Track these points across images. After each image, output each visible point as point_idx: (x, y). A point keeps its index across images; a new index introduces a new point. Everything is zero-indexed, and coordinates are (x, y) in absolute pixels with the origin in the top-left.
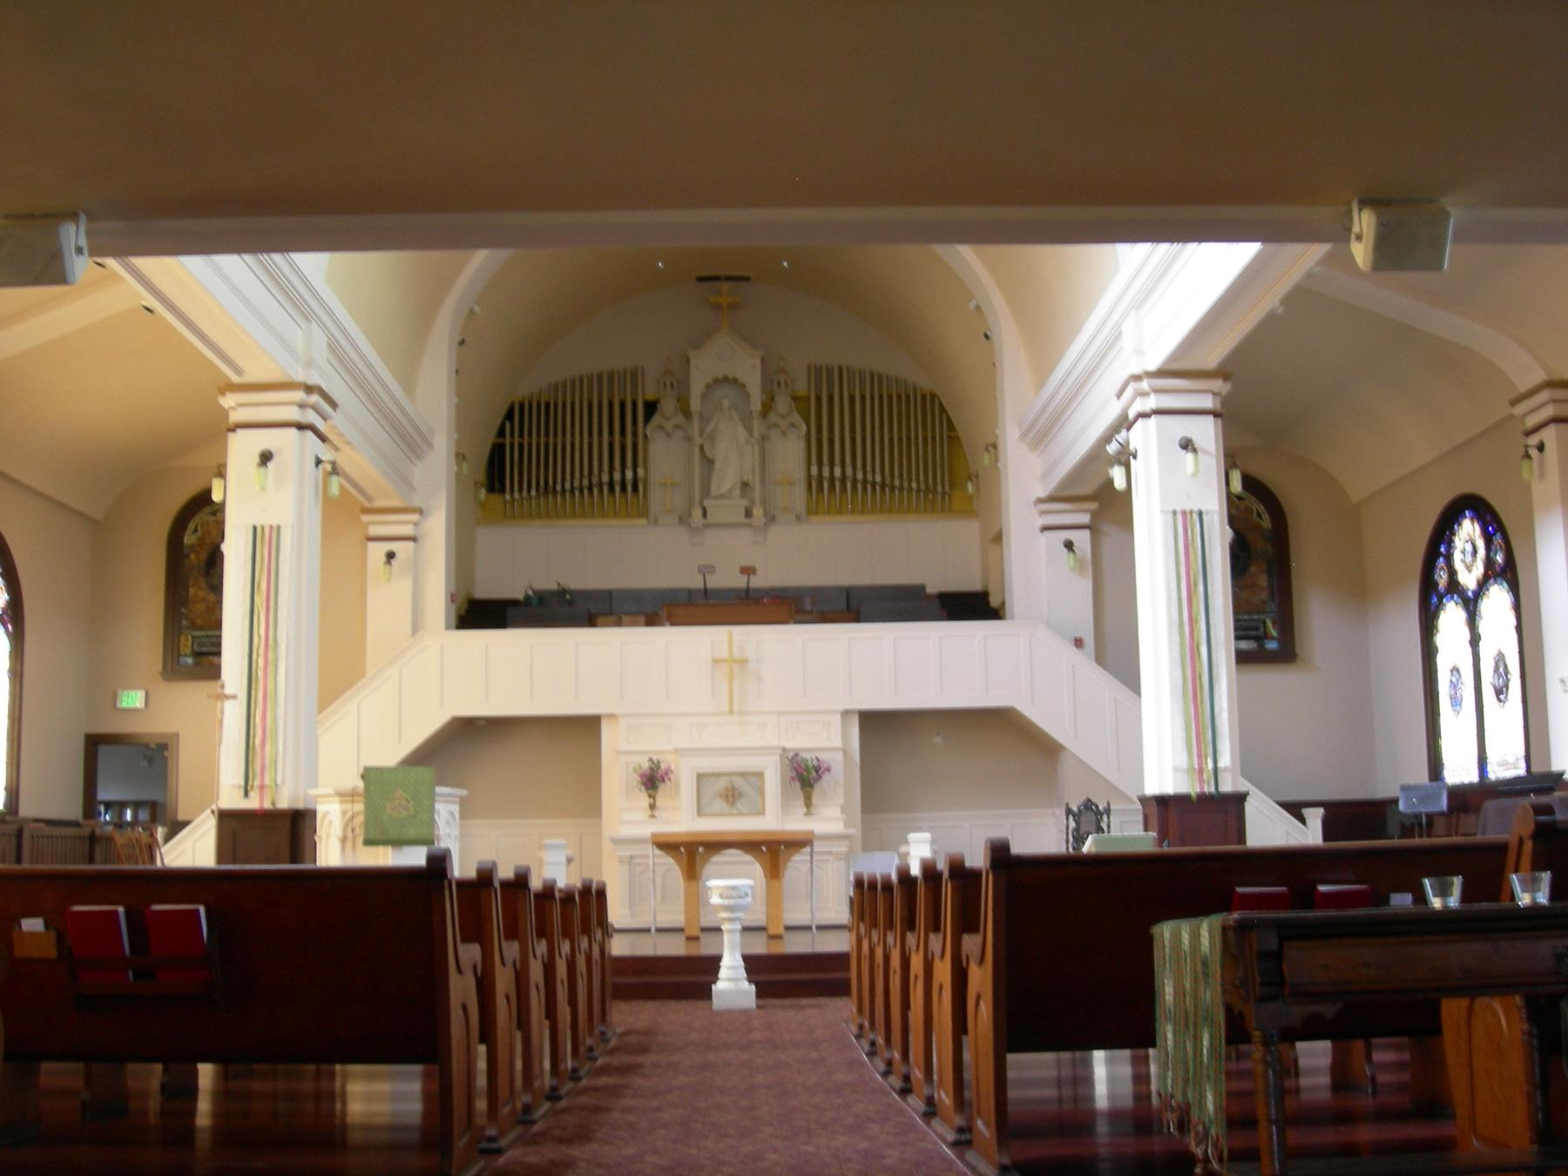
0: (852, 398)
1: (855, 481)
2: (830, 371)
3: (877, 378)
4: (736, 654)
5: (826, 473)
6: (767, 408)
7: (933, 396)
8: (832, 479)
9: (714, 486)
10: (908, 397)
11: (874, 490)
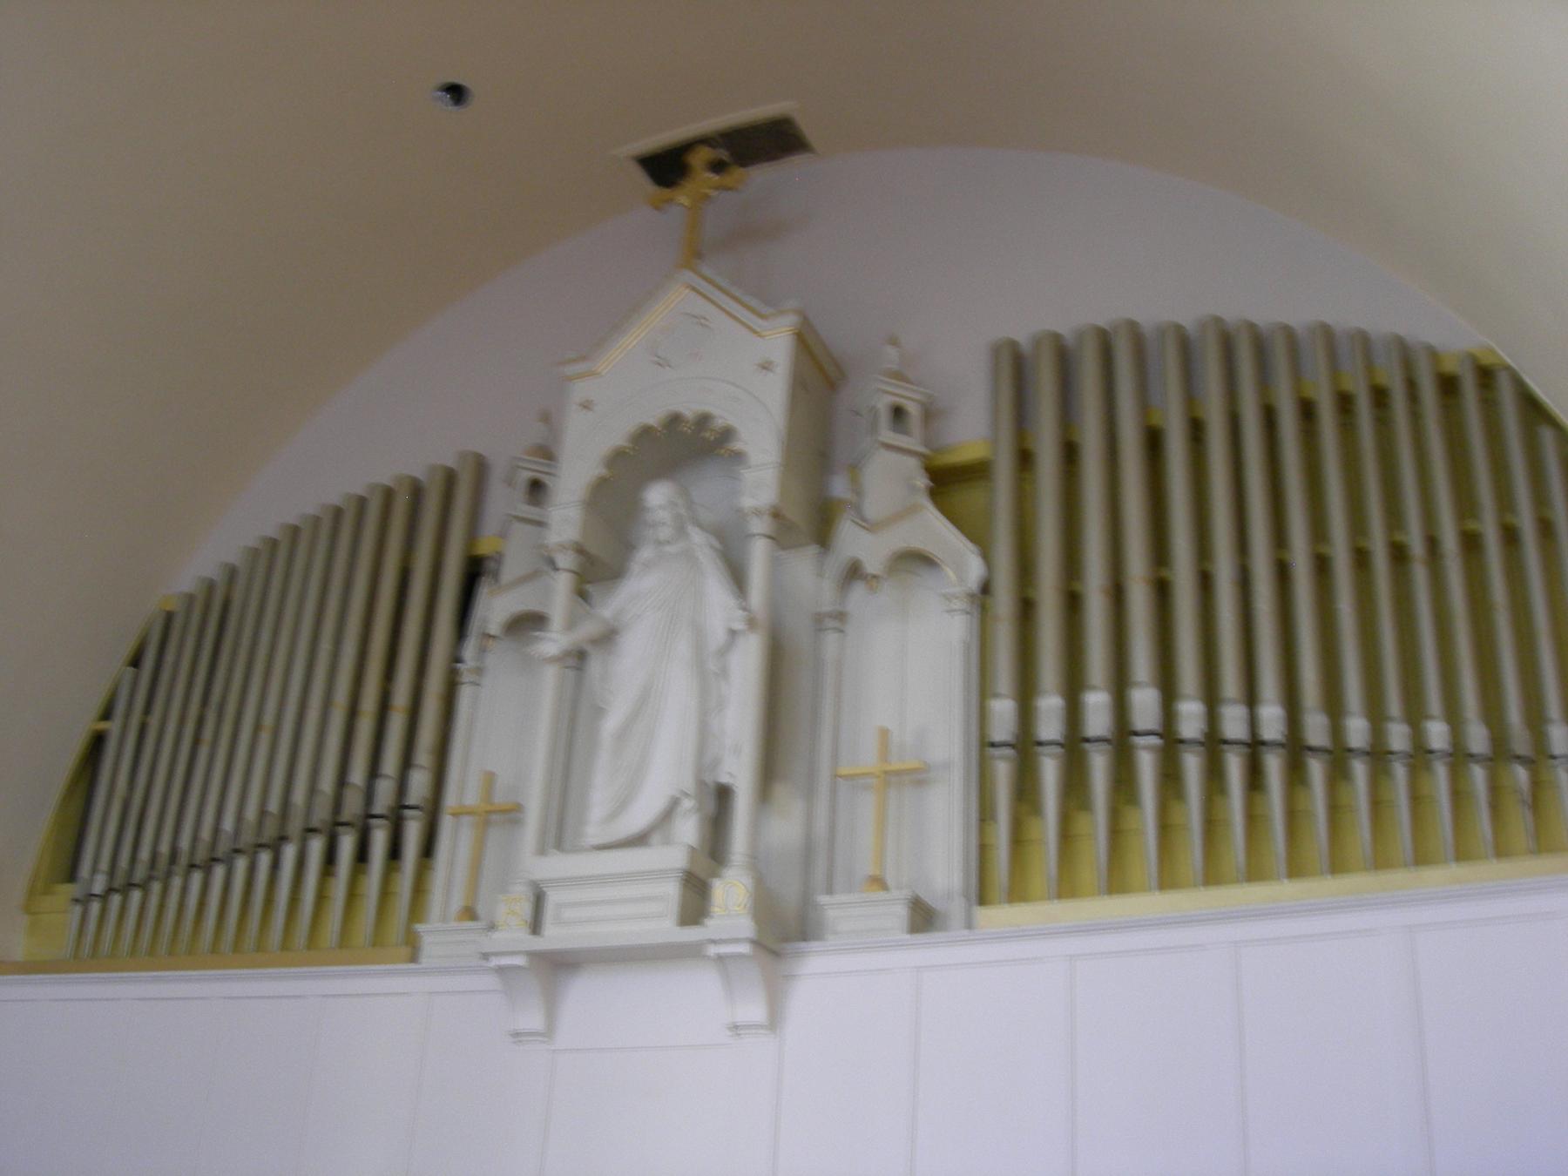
0: (1154, 442)
1: (1170, 743)
2: (1065, 359)
3: (1245, 350)
4: (499, 799)
5: (1050, 725)
6: (815, 518)
7: (1486, 375)
8: (1074, 744)
9: (600, 799)
10: (1380, 396)
11: (1255, 777)
